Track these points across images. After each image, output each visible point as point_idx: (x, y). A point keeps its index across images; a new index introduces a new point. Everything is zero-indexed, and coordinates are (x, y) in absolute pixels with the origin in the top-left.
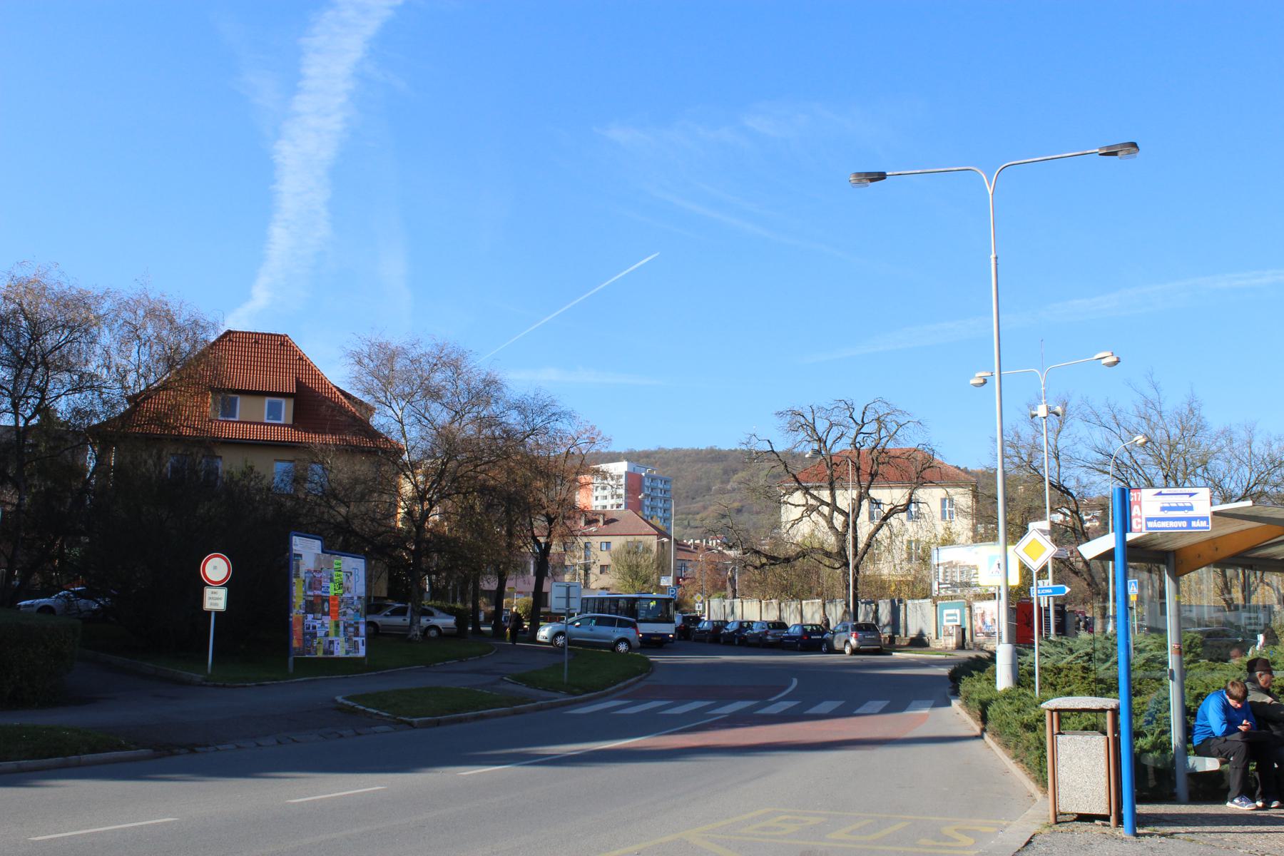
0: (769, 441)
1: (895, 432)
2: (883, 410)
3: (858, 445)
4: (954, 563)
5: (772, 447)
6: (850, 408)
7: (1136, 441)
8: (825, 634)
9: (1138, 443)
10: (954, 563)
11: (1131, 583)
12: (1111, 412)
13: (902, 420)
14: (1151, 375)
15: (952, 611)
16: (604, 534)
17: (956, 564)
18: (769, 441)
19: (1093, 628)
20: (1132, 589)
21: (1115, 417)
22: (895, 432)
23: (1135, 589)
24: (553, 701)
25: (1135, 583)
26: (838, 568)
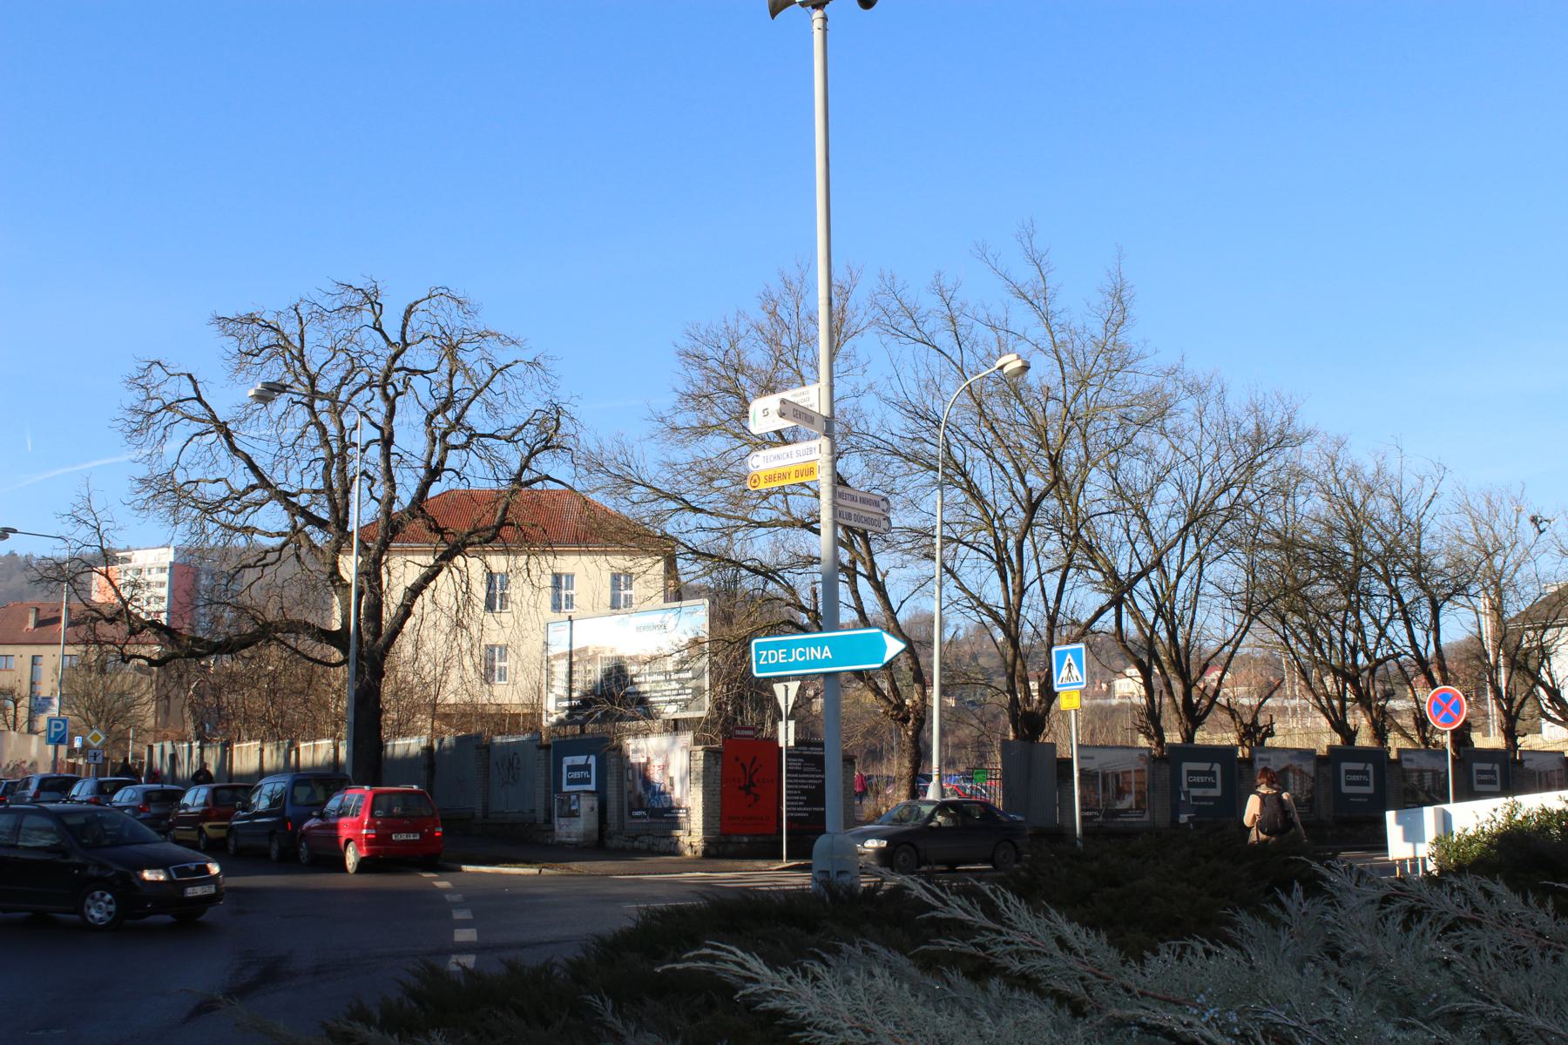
0: (190, 376)
1: (487, 385)
2: (454, 320)
3: (390, 390)
4: (590, 653)
5: (196, 390)
6: (372, 299)
7: (1001, 368)
8: (1305, 891)
9: (1006, 370)
10: (590, 653)
11: (1062, 655)
12: (945, 309)
13: (503, 356)
14: (1030, 237)
15: (580, 760)
16: (26, 641)
17: (595, 654)
18: (190, 376)
19: (1470, 640)
20: (1064, 673)
21: (953, 320)
22: (487, 385)
23: (1075, 671)
24: (1202, 803)
25: (1076, 654)
26: (338, 665)
